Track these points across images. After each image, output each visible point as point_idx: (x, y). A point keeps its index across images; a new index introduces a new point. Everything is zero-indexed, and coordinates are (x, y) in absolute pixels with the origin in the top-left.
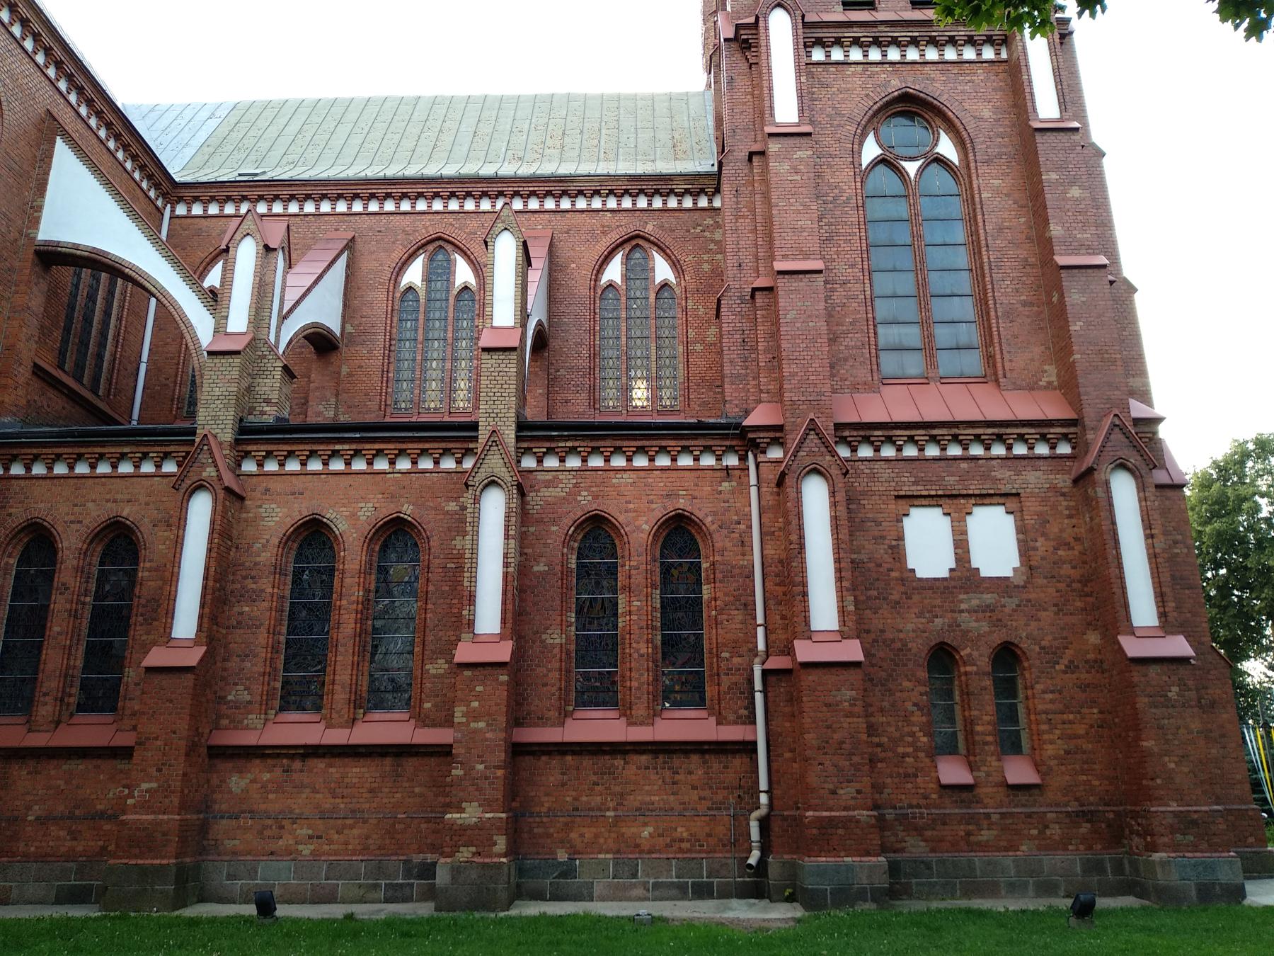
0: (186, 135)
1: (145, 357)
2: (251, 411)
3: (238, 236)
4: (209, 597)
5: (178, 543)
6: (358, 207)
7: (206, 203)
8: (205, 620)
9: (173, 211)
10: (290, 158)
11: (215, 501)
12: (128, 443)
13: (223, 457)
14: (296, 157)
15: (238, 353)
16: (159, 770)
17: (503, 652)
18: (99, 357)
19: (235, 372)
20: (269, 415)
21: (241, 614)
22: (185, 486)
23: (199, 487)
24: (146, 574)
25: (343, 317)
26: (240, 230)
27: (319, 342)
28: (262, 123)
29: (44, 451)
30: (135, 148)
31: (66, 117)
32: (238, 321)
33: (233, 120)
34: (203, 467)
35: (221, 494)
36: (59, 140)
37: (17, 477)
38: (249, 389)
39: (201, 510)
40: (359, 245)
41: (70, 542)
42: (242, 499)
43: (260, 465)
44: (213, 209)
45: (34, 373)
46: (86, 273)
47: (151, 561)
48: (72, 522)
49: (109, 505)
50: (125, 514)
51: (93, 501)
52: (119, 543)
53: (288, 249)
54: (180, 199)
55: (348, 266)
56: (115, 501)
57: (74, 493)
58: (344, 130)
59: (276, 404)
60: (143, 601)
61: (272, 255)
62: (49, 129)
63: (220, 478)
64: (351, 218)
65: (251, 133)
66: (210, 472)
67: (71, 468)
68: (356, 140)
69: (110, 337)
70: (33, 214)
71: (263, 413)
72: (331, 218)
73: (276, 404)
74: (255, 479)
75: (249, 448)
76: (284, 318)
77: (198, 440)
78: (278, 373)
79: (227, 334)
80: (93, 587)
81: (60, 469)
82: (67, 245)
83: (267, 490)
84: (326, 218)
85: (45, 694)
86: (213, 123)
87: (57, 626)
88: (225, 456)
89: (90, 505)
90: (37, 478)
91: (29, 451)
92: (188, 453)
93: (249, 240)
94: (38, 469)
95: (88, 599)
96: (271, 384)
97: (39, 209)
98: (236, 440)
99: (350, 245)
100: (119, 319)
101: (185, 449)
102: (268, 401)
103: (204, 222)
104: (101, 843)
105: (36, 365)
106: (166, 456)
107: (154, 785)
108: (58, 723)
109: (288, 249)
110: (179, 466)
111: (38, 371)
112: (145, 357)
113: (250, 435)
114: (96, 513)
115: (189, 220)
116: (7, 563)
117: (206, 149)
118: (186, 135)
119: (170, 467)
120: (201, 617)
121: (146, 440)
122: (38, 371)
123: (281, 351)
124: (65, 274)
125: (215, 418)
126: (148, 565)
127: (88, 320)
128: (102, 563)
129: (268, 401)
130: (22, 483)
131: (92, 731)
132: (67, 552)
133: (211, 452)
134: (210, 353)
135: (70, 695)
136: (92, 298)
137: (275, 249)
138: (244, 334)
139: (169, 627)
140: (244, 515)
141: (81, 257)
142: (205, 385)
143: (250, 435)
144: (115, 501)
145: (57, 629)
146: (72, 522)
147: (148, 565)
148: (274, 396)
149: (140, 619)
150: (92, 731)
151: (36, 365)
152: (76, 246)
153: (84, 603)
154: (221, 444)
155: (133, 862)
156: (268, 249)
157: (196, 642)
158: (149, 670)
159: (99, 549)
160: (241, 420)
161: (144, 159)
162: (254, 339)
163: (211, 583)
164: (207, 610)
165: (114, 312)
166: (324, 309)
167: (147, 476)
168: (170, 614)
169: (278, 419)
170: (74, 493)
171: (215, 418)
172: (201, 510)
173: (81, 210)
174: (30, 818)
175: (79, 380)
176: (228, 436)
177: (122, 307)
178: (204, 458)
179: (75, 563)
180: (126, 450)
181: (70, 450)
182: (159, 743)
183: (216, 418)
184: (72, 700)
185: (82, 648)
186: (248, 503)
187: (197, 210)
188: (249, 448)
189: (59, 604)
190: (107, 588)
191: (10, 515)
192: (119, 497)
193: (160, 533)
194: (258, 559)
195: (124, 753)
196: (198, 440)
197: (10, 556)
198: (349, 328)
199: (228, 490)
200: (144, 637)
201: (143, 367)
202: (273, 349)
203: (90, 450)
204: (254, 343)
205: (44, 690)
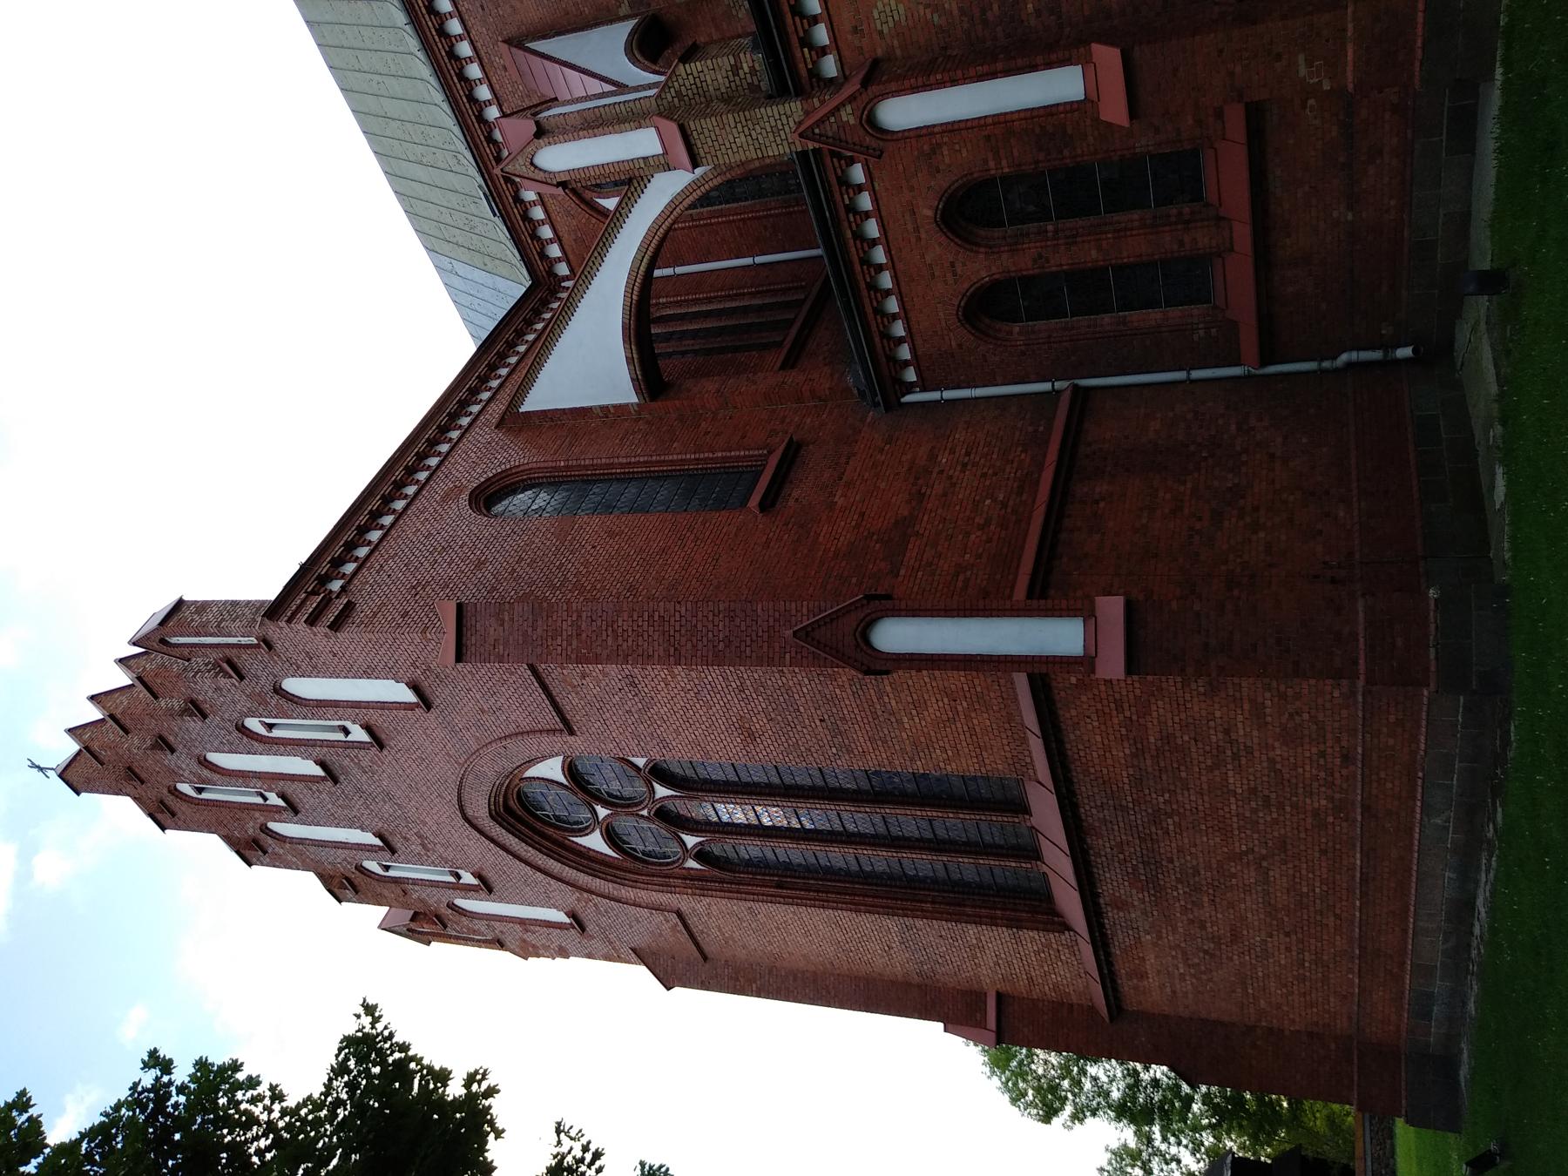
0: (487, 294)
1: (748, 261)
2: (754, 88)
3: (540, 176)
4: (1020, 62)
5: (953, 129)
6: (465, 49)
7: (544, 244)
8: (1054, 57)
9: (567, 278)
10: (452, 162)
11: (885, 96)
12: (840, 234)
13: (821, 105)
14: (449, 155)
15: (682, 128)
16: (1279, 57)
17: (1108, 57)
18: (760, 309)
19: (708, 123)
20: (752, 61)
21: (1038, 12)
22: (874, 143)
23: (871, 122)
24: (1004, 163)
25: (611, 22)
26: (531, 175)
27: (650, 44)
28: (433, 212)
29: (874, 328)
30: (509, 335)
31: (497, 409)
32: (642, 143)
33: (447, 248)
34: (843, 126)
35: (874, 89)
36: (523, 409)
37: (913, 350)
38: (727, 99)
39: (904, 112)
40: (511, 31)
41: (979, 269)
42: (876, 63)
43: (823, 51)
44: (546, 232)
45: (793, 367)
46: (659, 348)
47: (986, 161)
48: (955, 274)
49: (923, 236)
50: (930, 213)
51: (923, 256)
52: (968, 211)
53: (534, 110)
54: (551, 273)
55: (544, 37)
56: (917, 230)
57: (913, 275)
58: (393, 108)
59: (736, 57)
60: (1042, 156)
61: (545, 124)
62: (515, 422)
63: (852, 99)
64: (482, 53)
65: (449, 221)
66: (847, 115)
67: (888, 293)
68: (395, 86)
69: (734, 304)
70: (611, 415)
71: (753, 71)
72: (494, 80)
73: (736, 57)
74: (846, 53)
75: (804, 73)
76: (621, 88)
77: (811, 145)
78: (695, 67)
79: (666, 152)
80: (1033, 227)
81: (893, 305)
82: (633, 372)
83: (855, 30)
84: (497, 87)
85: (1181, 243)
86: (459, 267)
87: (1091, 255)
88: (822, 102)
89: (928, 259)
90: (908, 329)
91: (879, 346)
92: (833, 154)
93: (539, 161)
94: (899, 329)
95: (1050, 228)
96: (711, 72)
97: (605, 408)
98: (797, 95)
99: (517, 42)
100: (709, 300)
101: (828, 160)
102: (736, 69)
103: (565, 237)
104: (1387, 116)
105: (782, 368)
106: (845, 182)
107: (1301, 58)
108: (1219, 219)
109: (534, 110)
110: (851, 161)
111: (789, 363)
112: (748, 261)
113: (788, 76)
114: (938, 248)
115: (571, 257)
116: (1020, 333)
117: (489, 267)
118: (487, 294)
119: (858, 174)
120: (1049, 65)
121: (835, 225)
122: (785, 366)
123: (662, 78)
124: (668, 368)
125: (775, 131)
126: (992, 164)
127: (720, 331)
128: (1001, 224)
129: (736, 69)
130: (919, 342)
131: (1228, 178)
132: (994, 269)
133: (820, 122)
134: (695, 164)
135: (1180, 214)
136: (695, 334)
137: (537, 123)
138: (657, 129)
139: (1070, 107)
140: (898, 52)
141: (640, 352)
142: (737, 157)
143: (788, 76)
144: (917, 230)
145: (1094, 253)
146: (955, 274)
147: (992, 164)
148: (726, 62)
149: (1066, 153)
150: (1228, 178)
151: (782, 368)
152: (630, 361)
153: (1056, 231)
154: (807, 113)
155: (1419, 52)
156: (541, 132)
157: (1086, 61)
158: (1133, 113)
159: (982, 233)
160: (770, 97)
161: (518, 323)
162: (660, 115)
163: (999, 66)
164: (1039, 59)
165: (704, 308)
166: (605, 50)
167: (875, 200)
168: (1050, 111)
169: (755, 48)
170: (913, 275)
171: (775, 131)
172: (904, 112)
173: (589, 363)
174: (1350, 217)
175: (791, 323)
176: (795, 107)
177: (696, 302)
178: (830, 129)
179: (1005, 256)
180: (849, 234)
181: (867, 301)
182: (1238, 69)
183: (773, 133)
184: (1186, 210)
185: (1116, 217)
186: (879, 52)
187: (554, 251)
188: (804, 73)
189: (1060, 260)
190: (1031, 208)
191: (960, 346)
192: (910, 227)
193: (947, 160)
194: (956, 12)
195: (1255, 116)
196: (811, 145)
197: (1010, 333)
198: (624, 10)
199: (865, 83)
200: (1091, 139)
201: (759, 259)
202: (665, 87)
203: (860, 277)
204: (667, 113)
205: (1175, 247)
